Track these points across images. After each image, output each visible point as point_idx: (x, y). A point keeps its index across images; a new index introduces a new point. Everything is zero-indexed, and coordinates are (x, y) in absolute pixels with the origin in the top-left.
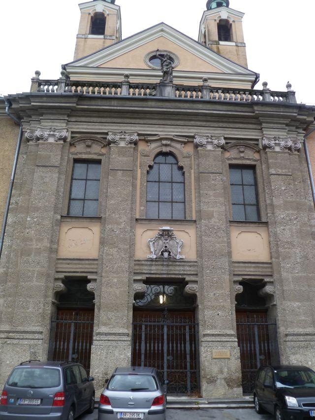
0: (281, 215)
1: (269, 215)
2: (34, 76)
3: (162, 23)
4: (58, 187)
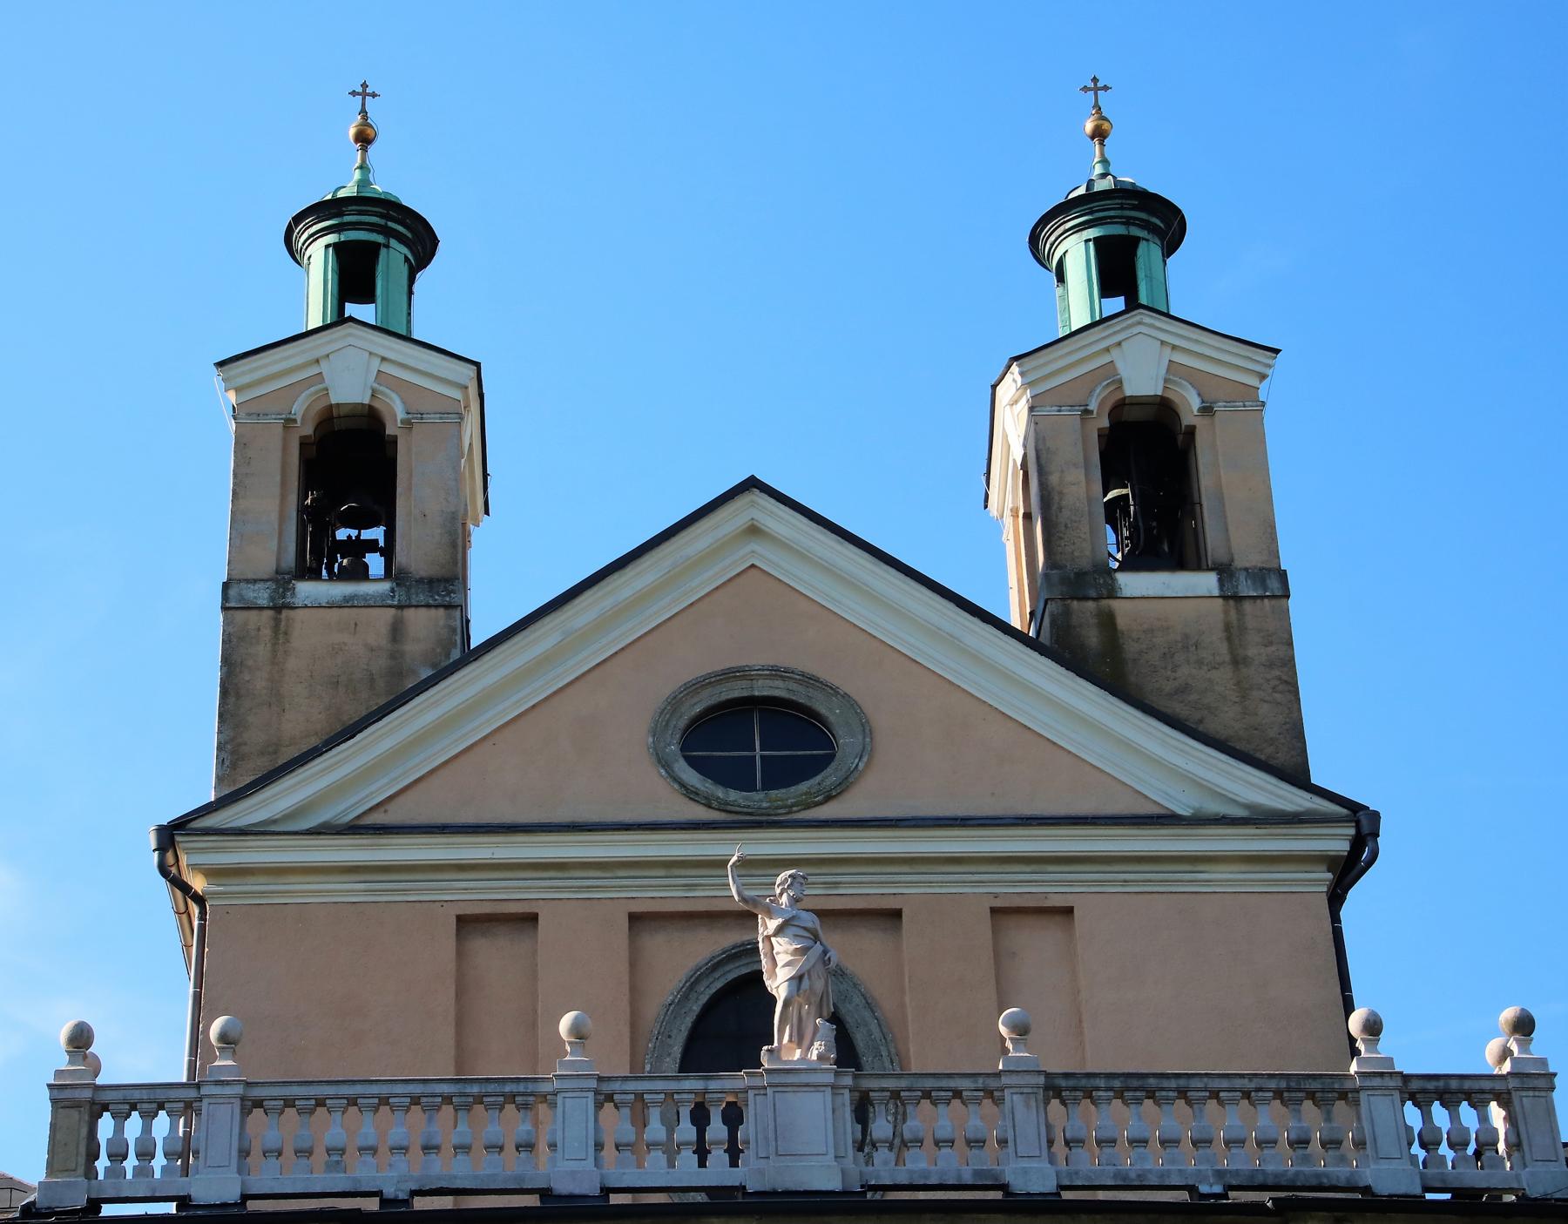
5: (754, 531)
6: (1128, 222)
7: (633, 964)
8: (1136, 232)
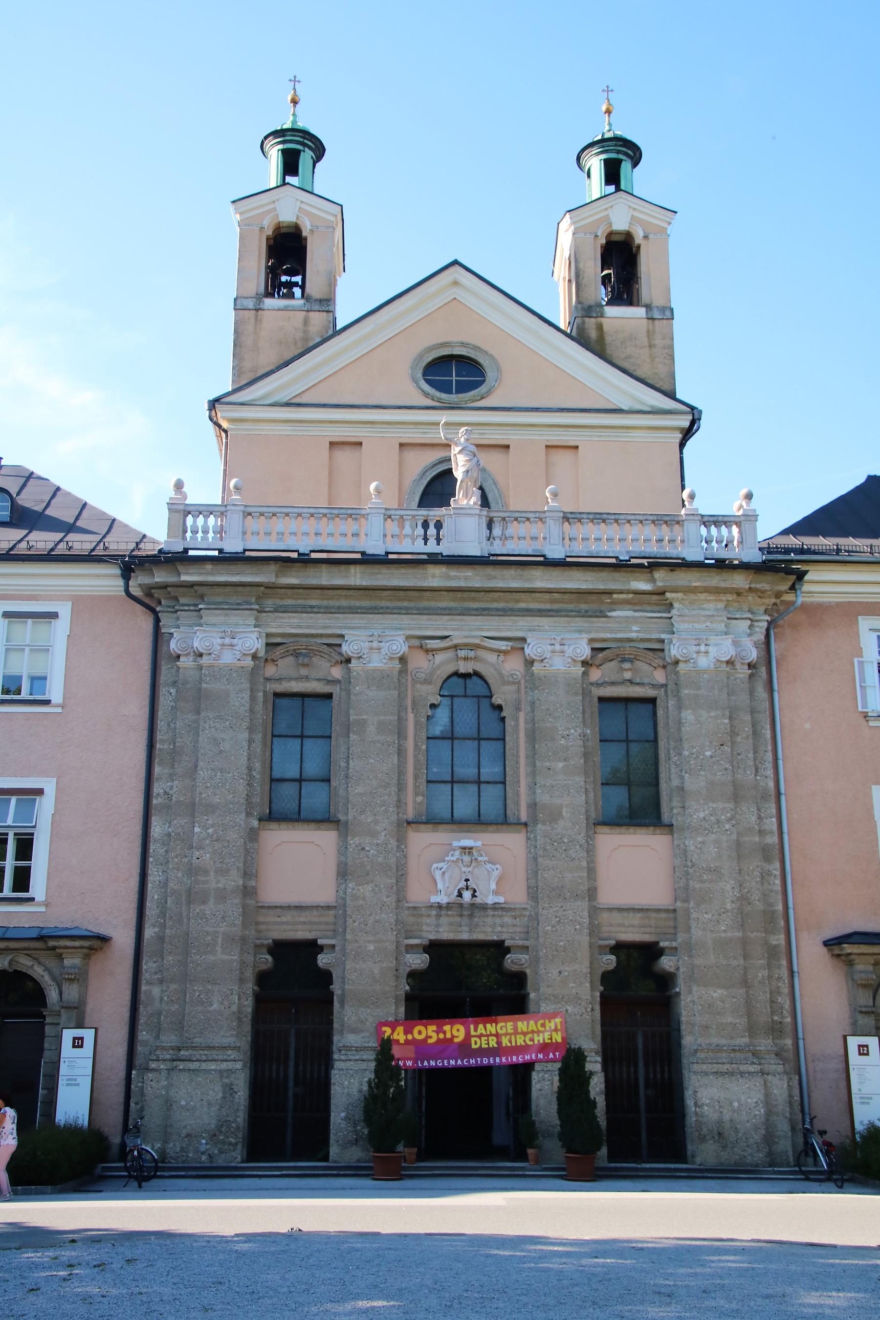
1: (675, 811)
2: (172, 494)
3: (456, 263)
4: (249, 759)
5: (456, 283)
6: (618, 152)
8: (621, 157)
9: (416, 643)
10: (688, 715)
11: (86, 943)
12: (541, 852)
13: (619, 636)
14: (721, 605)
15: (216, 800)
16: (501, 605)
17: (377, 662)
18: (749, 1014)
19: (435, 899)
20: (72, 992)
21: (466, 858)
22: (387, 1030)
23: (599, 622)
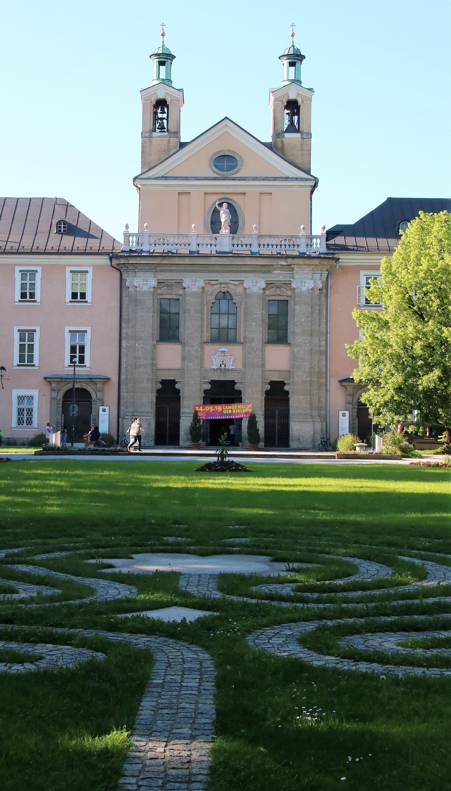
0: (299, 340)
5: (226, 125)
6: (295, 59)
7: (205, 200)
8: (296, 61)
9: (208, 282)
10: (297, 307)
11: (104, 380)
12: (247, 353)
13: (276, 279)
14: (311, 269)
15: (143, 335)
16: (236, 269)
17: (194, 289)
18: (311, 404)
19: (213, 367)
20: (100, 395)
21: (223, 354)
22: (198, 408)
23: (269, 275)
